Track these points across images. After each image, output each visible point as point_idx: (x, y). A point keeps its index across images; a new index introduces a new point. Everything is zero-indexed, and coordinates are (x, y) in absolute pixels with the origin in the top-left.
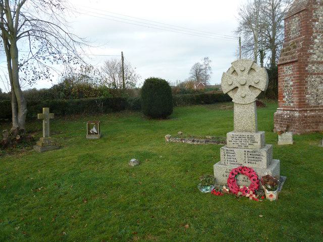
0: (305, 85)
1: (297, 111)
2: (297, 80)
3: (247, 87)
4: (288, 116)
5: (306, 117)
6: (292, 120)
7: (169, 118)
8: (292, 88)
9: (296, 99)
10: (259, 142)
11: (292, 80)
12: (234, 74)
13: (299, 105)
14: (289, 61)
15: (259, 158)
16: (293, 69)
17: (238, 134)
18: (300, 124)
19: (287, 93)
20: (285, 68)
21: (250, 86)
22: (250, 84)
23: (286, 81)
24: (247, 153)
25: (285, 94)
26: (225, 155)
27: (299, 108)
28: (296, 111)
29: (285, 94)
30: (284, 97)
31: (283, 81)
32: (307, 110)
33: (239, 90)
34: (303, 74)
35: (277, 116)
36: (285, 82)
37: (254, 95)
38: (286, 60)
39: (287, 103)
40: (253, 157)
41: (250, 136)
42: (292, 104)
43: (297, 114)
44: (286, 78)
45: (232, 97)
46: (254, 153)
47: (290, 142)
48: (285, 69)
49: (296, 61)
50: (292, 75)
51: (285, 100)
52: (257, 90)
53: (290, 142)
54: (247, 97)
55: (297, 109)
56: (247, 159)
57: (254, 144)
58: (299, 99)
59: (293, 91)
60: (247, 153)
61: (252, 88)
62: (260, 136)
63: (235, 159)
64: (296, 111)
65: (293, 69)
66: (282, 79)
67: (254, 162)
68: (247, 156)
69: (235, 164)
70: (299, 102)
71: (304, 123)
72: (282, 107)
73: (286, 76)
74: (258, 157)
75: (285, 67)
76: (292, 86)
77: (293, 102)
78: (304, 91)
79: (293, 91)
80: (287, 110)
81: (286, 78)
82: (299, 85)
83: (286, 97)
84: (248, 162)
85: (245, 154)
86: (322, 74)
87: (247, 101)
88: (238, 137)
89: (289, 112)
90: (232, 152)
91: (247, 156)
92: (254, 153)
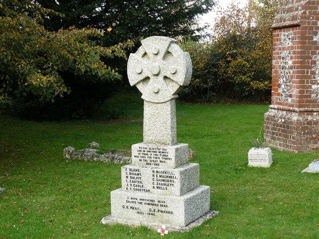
0: (311, 68)
2: (298, 58)
3: (161, 78)
4: (283, 120)
5: (309, 123)
6: (288, 127)
7: (114, 117)
8: (291, 71)
9: (295, 92)
10: (173, 158)
11: (292, 58)
12: (146, 58)
13: (299, 102)
14: (287, 23)
15: (171, 181)
16: (293, 39)
17: (146, 146)
18: (299, 134)
19: (285, 79)
20: (283, 35)
22: (165, 74)
23: (283, 58)
24: (155, 174)
25: (282, 80)
26: (127, 177)
27: (300, 106)
28: (294, 111)
30: (279, 86)
31: (280, 58)
32: (312, 111)
33: (151, 81)
34: (310, 48)
35: (268, 119)
36: (282, 60)
37: (170, 91)
38: (285, 21)
39: (283, 98)
40: (164, 180)
41: (161, 150)
42: (290, 100)
43: (295, 117)
45: (141, 91)
46: (164, 175)
47: (266, 164)
48: (283, 37)
49: (297, 26)
50: (292, 48)
51: (280, 91)
52: (172, 84)
53: (266, 164)
54: (161, 93)
56: (155, 182)
58: (301, 92)
59: (292, 77)
60: (155, 174)
61: (168, 81)
62: (174, 151)
63: (141, 182)
64: (294, 111)
65: (293, 39)
66: (278, 53)
67: (165, 187)
68: (155, 178)
70: (300, 97)
71: (307, 134)
72: (277, 103)
73: (284, 49)
74: (169, 179)
75: (283, 33)
76: (291, 68)
77: (291, 96)
78: (309, 77)
79: (292, 77)
80: (283, 110)
82: (301, 67)
83: (283, 86)
84: (157, 187)
85: (153, 176)
87: (160, 98)
88: (146, 150)
89: (285, 113)
90: (137, 172)
91: (155, 178)
92: (164, 175)
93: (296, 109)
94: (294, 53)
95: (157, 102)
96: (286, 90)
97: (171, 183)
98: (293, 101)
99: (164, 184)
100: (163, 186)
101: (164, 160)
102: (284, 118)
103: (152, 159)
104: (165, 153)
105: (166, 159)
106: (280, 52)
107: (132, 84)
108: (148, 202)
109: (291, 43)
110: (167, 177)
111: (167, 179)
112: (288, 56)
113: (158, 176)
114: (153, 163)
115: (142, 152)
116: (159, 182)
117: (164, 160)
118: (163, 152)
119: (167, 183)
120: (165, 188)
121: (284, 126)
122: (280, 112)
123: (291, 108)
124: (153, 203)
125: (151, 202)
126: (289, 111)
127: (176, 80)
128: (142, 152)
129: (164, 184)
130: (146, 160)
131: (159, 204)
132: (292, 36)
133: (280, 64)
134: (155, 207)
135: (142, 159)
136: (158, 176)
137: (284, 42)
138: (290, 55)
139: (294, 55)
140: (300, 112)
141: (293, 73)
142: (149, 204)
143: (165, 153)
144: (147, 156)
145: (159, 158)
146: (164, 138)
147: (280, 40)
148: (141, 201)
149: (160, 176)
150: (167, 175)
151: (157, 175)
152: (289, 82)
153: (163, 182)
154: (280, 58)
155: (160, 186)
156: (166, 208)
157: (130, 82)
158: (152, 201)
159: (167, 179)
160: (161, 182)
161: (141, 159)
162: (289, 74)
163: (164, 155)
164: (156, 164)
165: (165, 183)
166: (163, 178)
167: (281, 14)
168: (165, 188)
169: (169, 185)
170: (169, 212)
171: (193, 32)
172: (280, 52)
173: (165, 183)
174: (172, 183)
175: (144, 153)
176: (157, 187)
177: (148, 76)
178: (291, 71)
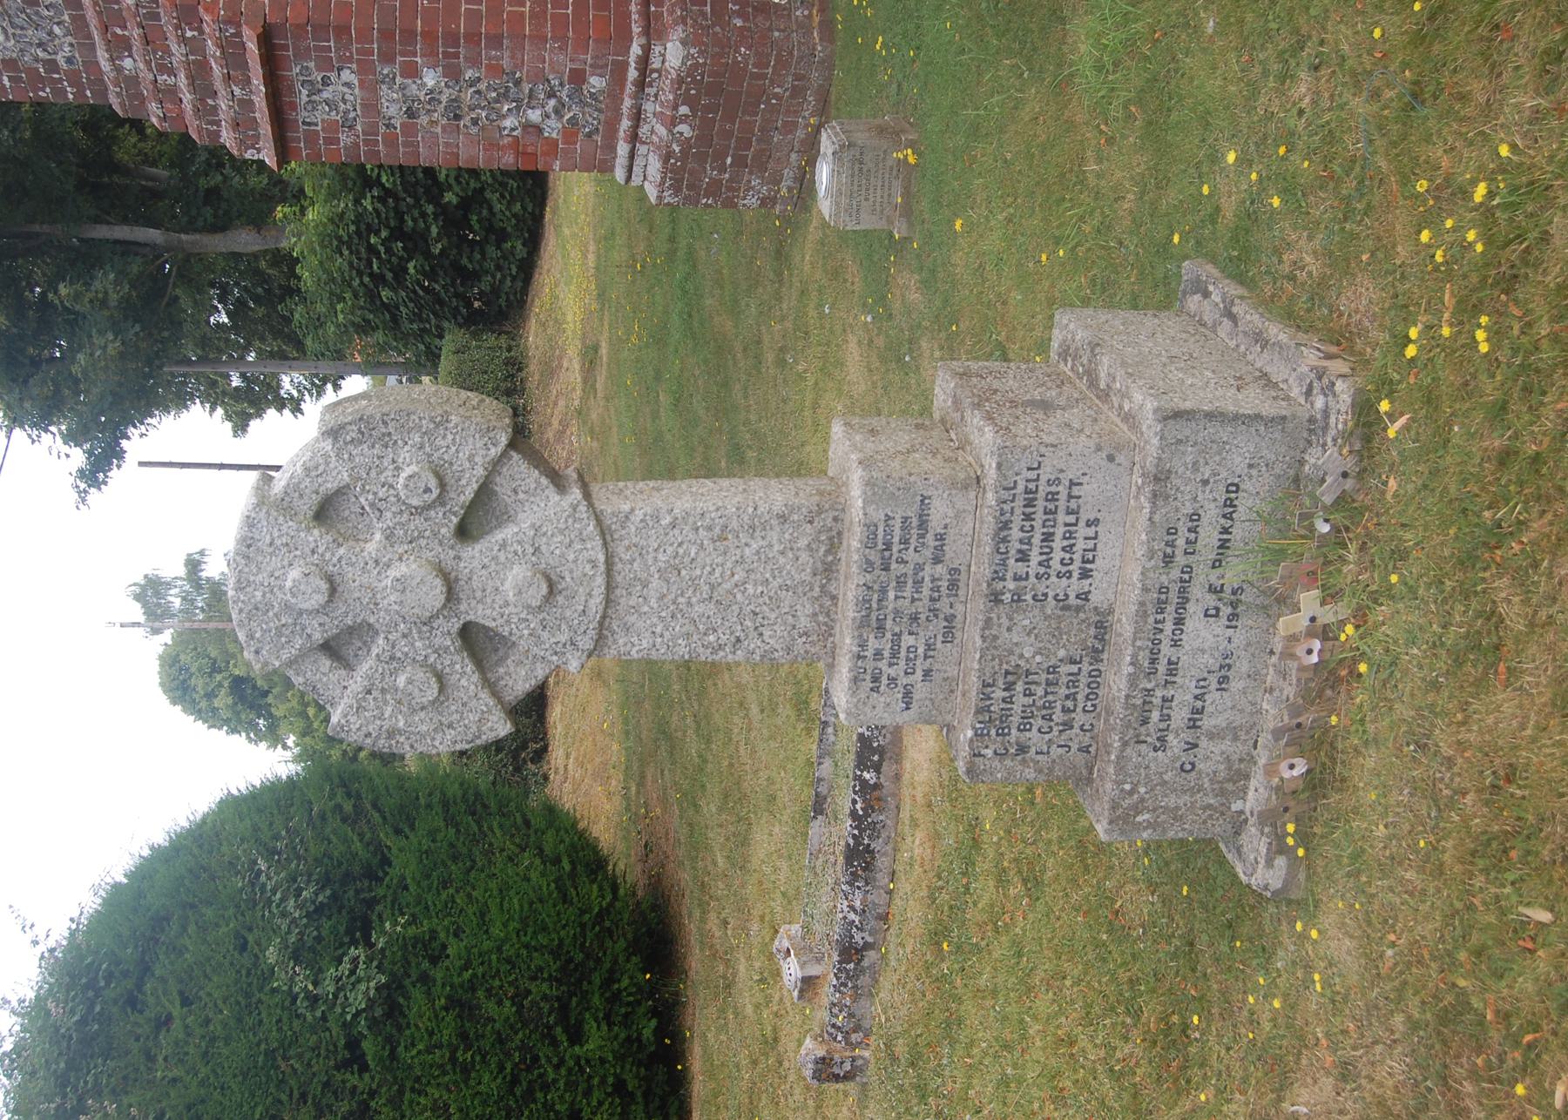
1: (647, 50)
11: (412, 72)
21: (464, 532)
23: (411, 113)
28: (644, 61)
29: (508, 123)
31: (410, 130)
33: (481, 614)
36: (423, 120)
40: (1048, 537)
42: (596, 83)
44: (392, 108)
47: (1062, 318)
48: (320, 116)
50: (365, 69)
52: (503, 487)
55: (636, 50)
57: (935, 523)
63: (1052, 670)
64: (644, 61)
65: (326, 64)
66: (391, 141)
67: (1082, 531)
69: (1001, 538)
73: (371, 107)
74: (1041, 504)
76: (453, 74)
77: (578, 78)
80: (637, 117)
81: (392, 108)
83: (534, 116)
84: (1085, 574)
86: (824, 1118)
88: (873, 644)
92: (1015, 533)
93: (636, 50)
94: (388, 58)
95: (600, 580)
96: (552, 102)
97: (1063, 496)
98: (598, 68)
99: (1069, 536)
100: (1081, 545)
101: (930, 539)
102: (675, 108)
103: (922, 607)
104: (889, 532)
105: (923, 524)
106: (382, 129)
107: (501, 727)
108: (1169, 627)
109: (347, 75)
110: (1028, 517)
111: (1040, 516)
112: (403, 88)
113: (1021, 568)
114: (944, 605)
115: (883, 665)
116: (1055, 564)
117: (930, 537)
118: (888, 546)
119: (1062, 517)
120: (1091, 532)
121: (707, 109)
122: (644, 130)
123: (632, 74)
124: (1173, 597)
125: (1170, 609)
126: (641, 84)
127: (480, 472)
128: (883, 665)
129: (1069, 536)
130: (929, 647)
131: (1180, 559)
132: (312, 64)
133: (439, 130)
134: (1197, 591)
135: (920, 666)
136: (1021, 568)
137: (342, 107)
138: (398, 80)
139: (399, 59)
140: (647, 32)
141: (475, 62)
142: (1179, 622)
143: (889, 532)
144: (907, 640)
145: (919, 567)
146: (803, 542)
147: (332, 127)
148: (1162, 668)
149: (1023, 557)
150: (1017, 520)
151: (1017, 578)
152: (518, 83)
153: (1058, 543)
154: (410, 130)
155: (1077, 557)
156: (1205, 520)
157: (488, 737)
158: (1160, 607)
159: (1040, 516)
160: (1058, 555)
161: (919, 674)
162: (482, 86)
163: (905, 541)
164: (953, 585)
165: (1060, 531)
166: (1037, 540)
167: (218, 123)
168: (1091, 532)
169: (1073, 504)
170: (1230, 503)
171: (527, 1107)
172: (382, 129)
173: (1060, 531)
174: (1063, 490)
175: (886, 654)
176: (1085, 574)
177: (458, 626)
178: (469, 74)
